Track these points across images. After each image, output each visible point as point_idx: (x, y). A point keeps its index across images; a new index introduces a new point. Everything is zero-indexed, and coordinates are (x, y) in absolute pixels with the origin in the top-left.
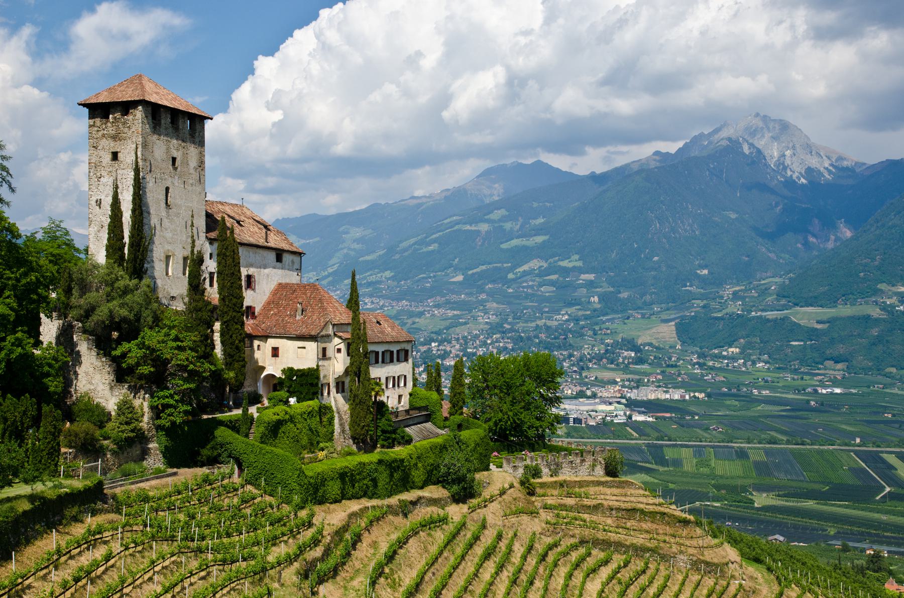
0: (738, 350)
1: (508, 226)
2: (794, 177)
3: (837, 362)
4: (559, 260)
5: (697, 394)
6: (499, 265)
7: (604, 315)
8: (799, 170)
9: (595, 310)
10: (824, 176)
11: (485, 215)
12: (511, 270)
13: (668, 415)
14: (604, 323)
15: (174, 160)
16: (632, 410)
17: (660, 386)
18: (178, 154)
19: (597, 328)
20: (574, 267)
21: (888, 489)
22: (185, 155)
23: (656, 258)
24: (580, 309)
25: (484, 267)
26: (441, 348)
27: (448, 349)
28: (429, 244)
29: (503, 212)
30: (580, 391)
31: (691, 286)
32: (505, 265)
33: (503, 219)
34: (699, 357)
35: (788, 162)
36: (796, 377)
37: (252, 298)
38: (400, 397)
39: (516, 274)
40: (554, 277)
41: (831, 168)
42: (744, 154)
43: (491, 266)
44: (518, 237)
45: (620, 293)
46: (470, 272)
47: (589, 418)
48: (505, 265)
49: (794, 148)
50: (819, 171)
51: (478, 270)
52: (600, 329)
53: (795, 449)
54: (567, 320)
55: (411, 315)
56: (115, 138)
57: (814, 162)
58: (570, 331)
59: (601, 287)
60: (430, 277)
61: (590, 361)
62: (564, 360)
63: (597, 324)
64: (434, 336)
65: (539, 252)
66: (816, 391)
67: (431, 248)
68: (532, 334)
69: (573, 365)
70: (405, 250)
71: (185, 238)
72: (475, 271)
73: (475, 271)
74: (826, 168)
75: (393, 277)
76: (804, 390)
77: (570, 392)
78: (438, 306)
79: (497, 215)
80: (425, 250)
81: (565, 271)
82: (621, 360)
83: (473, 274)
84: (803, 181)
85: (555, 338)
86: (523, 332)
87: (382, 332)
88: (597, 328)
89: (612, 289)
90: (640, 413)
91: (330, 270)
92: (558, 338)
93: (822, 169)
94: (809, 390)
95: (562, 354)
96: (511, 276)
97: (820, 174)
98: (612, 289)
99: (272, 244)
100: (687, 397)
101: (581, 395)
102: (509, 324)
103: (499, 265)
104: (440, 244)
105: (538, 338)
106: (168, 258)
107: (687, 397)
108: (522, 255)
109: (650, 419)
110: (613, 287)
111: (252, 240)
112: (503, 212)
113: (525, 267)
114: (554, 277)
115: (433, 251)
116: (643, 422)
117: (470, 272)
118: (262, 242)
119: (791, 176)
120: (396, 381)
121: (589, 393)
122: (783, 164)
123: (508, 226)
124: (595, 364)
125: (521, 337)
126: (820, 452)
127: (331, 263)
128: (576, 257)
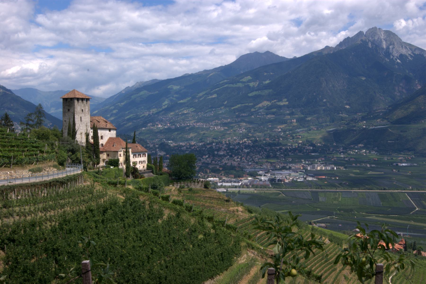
0: (363, 145)
1: (251, 84)
2: (394, 58)
3: (410, 151)
4: (277, 101)
5: (340, 167)
6: (247, 104)
7: (298, 129)
8: (396, 55)
9: (294, 126)
10: (408, 58)
11: (240, 79)
12: (253, 106)
13: (324, 177)
14: (298, 133)
15: (82, 110)
16: (307, 175)
17: (323, 164)
18: (83, 109)
19: (294, 135)
20: (284, 105)
21: (417, 209)
22: (85, 109)
23: (325, 100)
24: (286, 126)
25: (239, 105)
26: (217, 146)
27: (221, 146)
28: (212, 94)
29: (249, 78)
30: (283, 166)
31: (342, 114)
32: (250, 104)
33: (250, 81)
34: (343, 149)
35: (391, 51)
36: (389, 158)
37: (101, 142)
38: (144, 166)
39: (255, 108)
40: (274, 110)
41: (412, 54)
42: (369, 48)
43: (243, 105)
44: (256, 90)
45: (306, 117)
46: (233, 108)
47: (285, 179)
48: (250, 104)
49: (394, 44)
50: (406, 56)
51: (237, 107)
52: (296, 136)
53: (380, 192)
54: (280, 132)
55: (203, 129)
56: (69, 106)
57: (404, 51)
58: (281, 137)
59: (297, 115)
60: (213, 111)
61: (290, 151)
62: (277, 151)
63: (295, 133)
64: (215, 140)
65: (269, 98)
66: (397, 165)
67: (213, 96)
68: (262, 138)
69: (282, 154)
70: (201, 97)
71: (85, 128)
72: (235, 107)
73: (235, 107)
74: (410, 55)
75: (194, 111)
76: (392, 164)
77: (278, 167)
78: (216, 125)
79: (245, 79)
80: (210, 97)
81: (280, 107)
82: (305, 151)
83: (234, 109)
84: (399, 61)
85: (273, 141)
86: (258, 137)
87: (138, 149)
88: (294, 135)
89: (303, 116)
90: (310, 176)
91: (164, 107)
92: (275, 140)
93: (407, 55)
94: (394, 164)
95: (276, 148)
96: (253, 110)
97: (407, 57)
98: (303, 116)
99: (108, 127)
100: (335, 168)
101: (284, 168)
102: (251, 133)
103: (247, 104)
104: (218, 94)
105: (265, 140)
106: (81, 133)
107: (335, 168)
108: (258, 99)
109: (315, 179)
110: (303, 115)
111: (102, 127)
112: (249, 78)
113: (260, 105)
114: (274, 110)
115: (214, 98)
116: (311, 181)
117: (233, 108)
118: (105, 127)
119: (393, 58)
120: (141, 162)
121: (288, 167)
122: (389, 52)
123: (251, 84)
124: (292, 153)
125: (257, 140)
126: (391, 193)
127: (164, 104)
128: (286, 100)
